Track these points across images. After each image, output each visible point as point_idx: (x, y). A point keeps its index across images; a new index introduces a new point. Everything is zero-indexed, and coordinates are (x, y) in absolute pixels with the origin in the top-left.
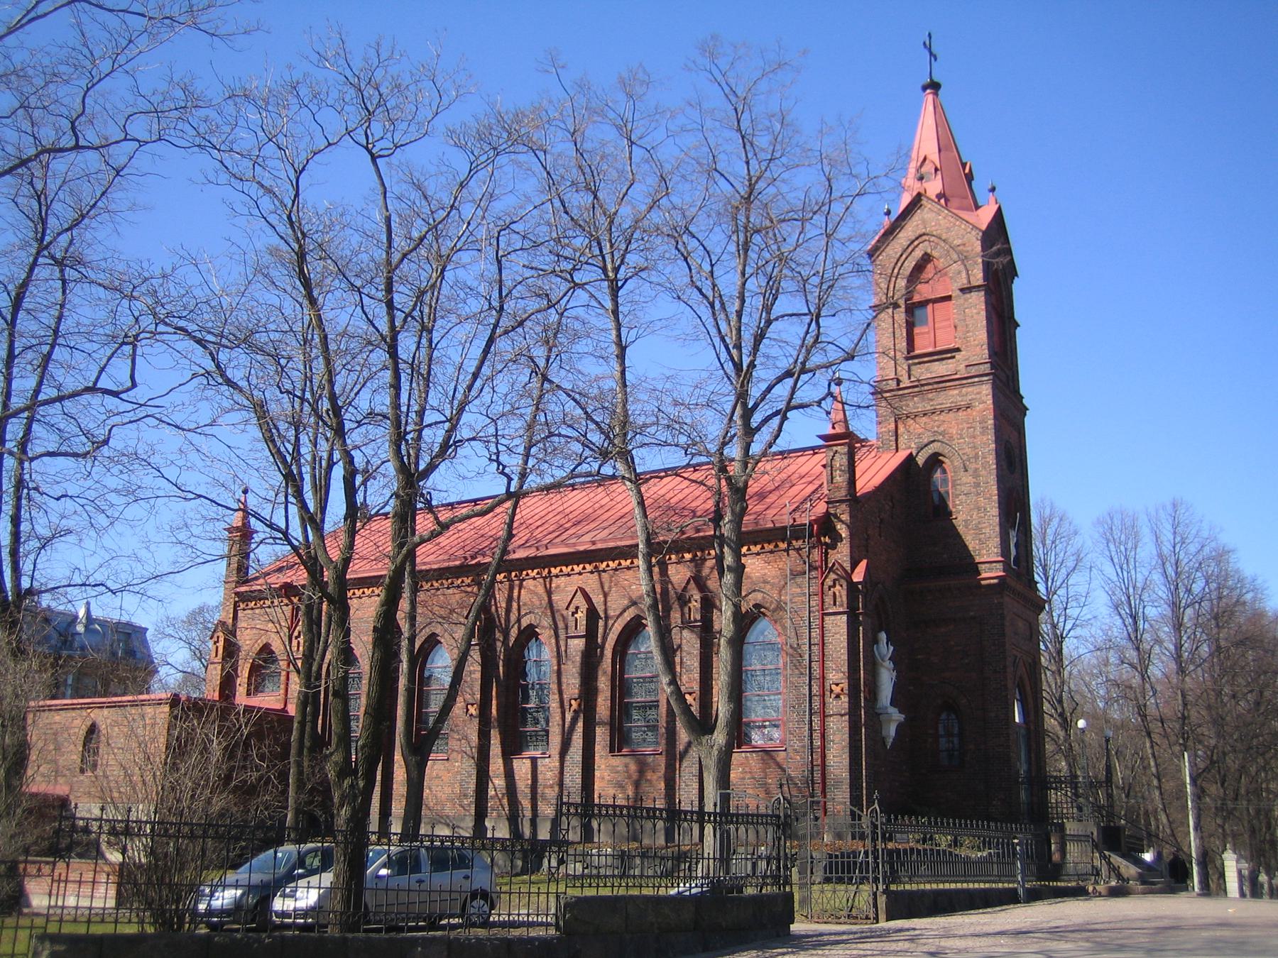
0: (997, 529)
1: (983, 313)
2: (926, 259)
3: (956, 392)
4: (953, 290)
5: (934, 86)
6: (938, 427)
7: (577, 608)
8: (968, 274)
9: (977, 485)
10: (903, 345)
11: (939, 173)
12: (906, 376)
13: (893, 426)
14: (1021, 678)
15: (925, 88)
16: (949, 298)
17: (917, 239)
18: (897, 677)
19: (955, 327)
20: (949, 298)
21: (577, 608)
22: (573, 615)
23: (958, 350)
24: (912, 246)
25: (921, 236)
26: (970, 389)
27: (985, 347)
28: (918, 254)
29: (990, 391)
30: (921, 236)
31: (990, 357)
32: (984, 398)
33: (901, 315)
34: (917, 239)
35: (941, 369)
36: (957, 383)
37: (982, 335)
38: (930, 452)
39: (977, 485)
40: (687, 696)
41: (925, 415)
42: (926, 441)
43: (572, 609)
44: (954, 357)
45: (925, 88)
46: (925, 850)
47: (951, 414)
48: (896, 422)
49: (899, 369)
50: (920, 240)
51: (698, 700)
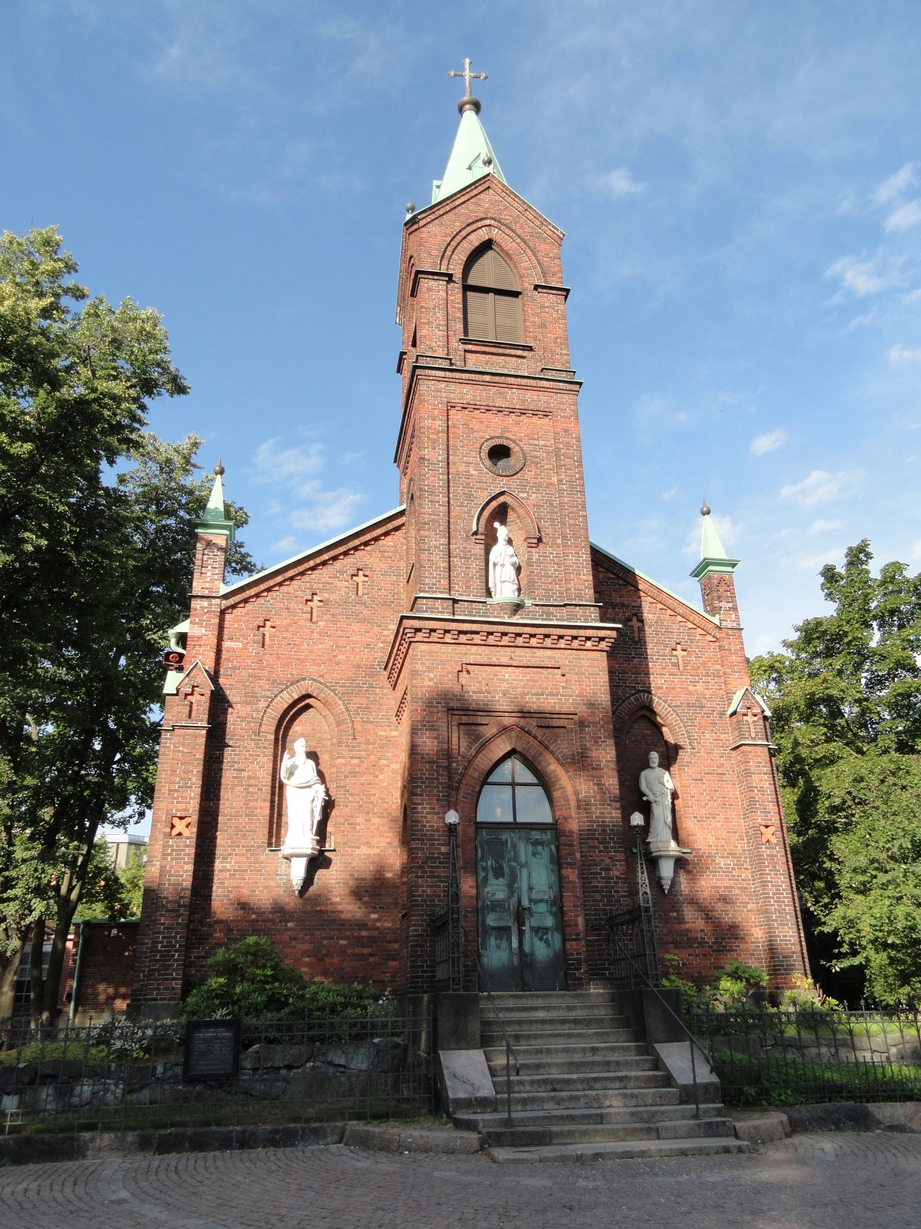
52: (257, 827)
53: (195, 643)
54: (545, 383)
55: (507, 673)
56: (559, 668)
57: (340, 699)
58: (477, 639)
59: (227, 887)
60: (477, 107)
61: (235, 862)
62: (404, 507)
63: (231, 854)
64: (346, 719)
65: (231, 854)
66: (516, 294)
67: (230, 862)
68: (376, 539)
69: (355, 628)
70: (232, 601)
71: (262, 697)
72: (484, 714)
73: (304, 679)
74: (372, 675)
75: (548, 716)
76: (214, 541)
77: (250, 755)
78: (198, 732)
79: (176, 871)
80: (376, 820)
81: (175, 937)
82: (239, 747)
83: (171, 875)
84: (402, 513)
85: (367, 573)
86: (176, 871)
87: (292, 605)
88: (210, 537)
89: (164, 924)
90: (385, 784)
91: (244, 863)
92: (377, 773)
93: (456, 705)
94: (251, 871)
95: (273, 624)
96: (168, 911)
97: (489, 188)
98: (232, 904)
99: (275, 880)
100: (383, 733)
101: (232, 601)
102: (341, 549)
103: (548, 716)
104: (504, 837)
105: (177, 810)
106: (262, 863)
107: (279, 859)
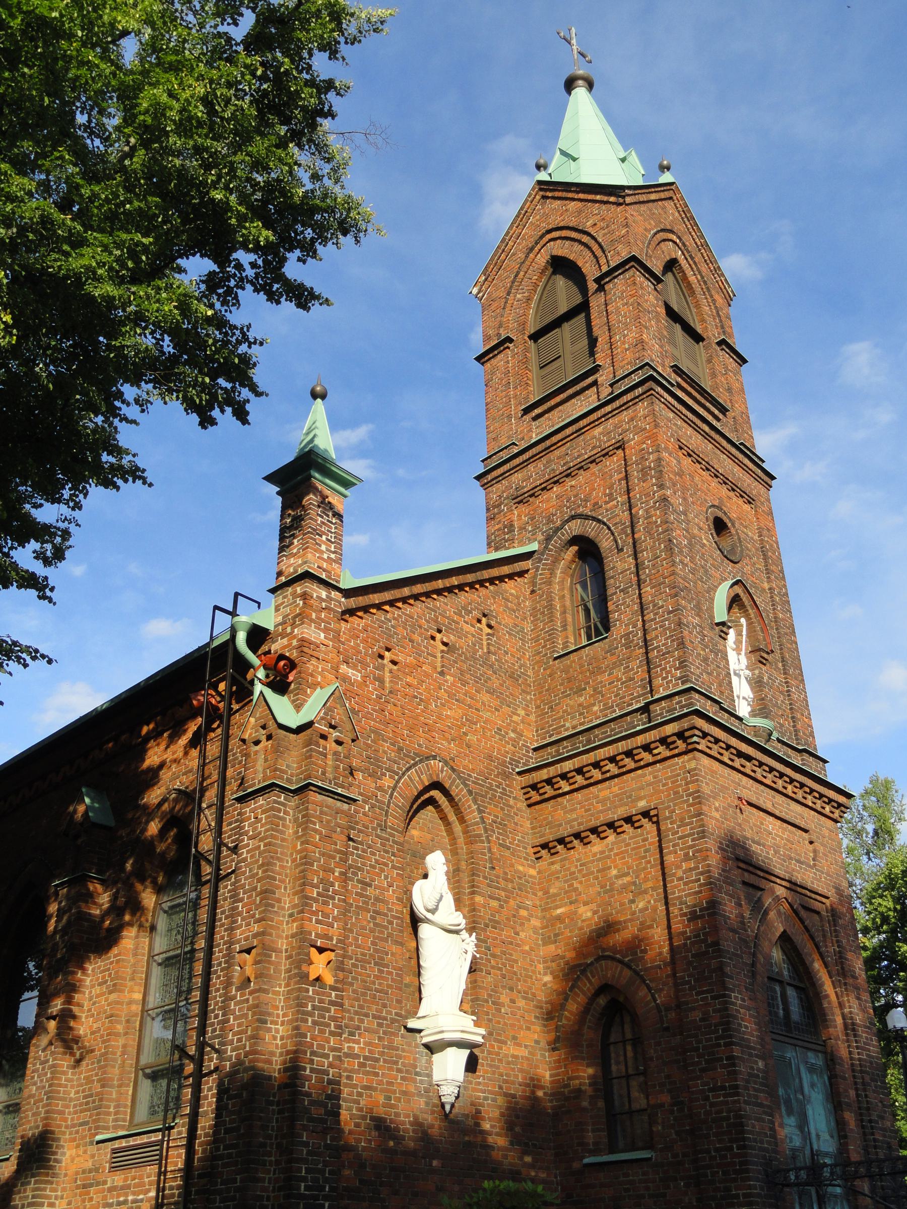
52: (389, 986)
53: (311, 652)
54: (746, 461)
55: (771, 824)
56: (806, 831)
57: (475, 801)
58: (749, 767)
59: (356, 1086)
60: (590, 85)
61: (365, 1043)
62: (534, 546)
63: (359, 1028)
64: (480, 836)
65: (359, 1028)
66: (698, 338)
67: (358, 1042)
68: (501, 579)
69: (485, 699)
70: (362, 601)
71: (388, 770)
72: (762, 874)
73: (434, 758)
74: (506, 776)
75: (808, 893)
76: (330, 499)
77: (377, 861)
78: (339, 804)
79: (319, 1046)
80: (521, 1003)
81: (322, 1172)
82: (361, 843)
83: (313, 1053)
84: (528, 555)
85: (493, 623)
86: (319, 1046)
87: (416, 637)
88: (327, 492)
89: (306, 1144)
90: (527, 948)
91: (377, 1046)
92: (518, 928)
93: (740, 853)
94: (385, 1061)
95: (395, 658)
96: (311, 1119)
97: (671, 198)
98: (364, 1118)
99: (415, 1081)
100: (521, 868)
101: (362, 601)
102: (470, 578)
103: (808, 893)
104: (788, 1055)
105: (317, 935)
106: (397, 1049)
107: (417, 1046)
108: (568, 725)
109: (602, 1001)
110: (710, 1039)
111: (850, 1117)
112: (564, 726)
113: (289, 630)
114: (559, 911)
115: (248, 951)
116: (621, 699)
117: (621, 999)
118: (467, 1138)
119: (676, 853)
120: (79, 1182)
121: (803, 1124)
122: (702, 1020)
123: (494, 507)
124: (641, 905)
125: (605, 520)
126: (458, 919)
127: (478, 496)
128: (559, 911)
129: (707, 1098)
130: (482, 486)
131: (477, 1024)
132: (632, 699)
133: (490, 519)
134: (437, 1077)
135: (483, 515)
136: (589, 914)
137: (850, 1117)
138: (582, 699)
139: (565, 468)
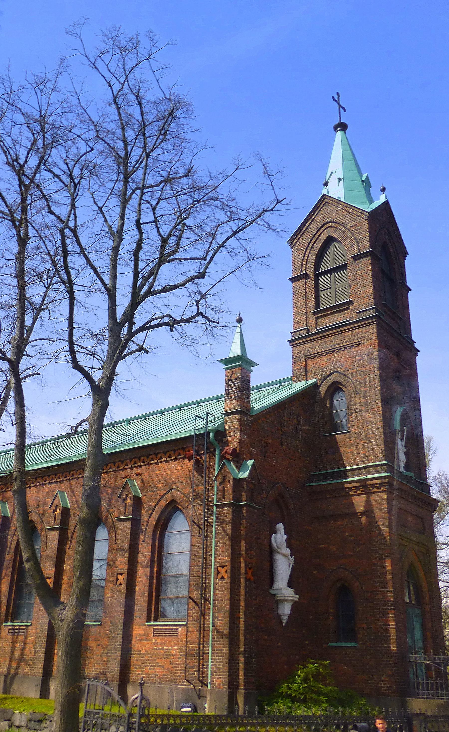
0: (382, 438)
1: (370, 273)
2: (330, 240)
3: (350, 333)
4: (347, 259)
5: (342, 127)
6: (337, 361)
7: (56, 507)
8: (358, 245)
9: (366, 404)
10: (312, 303)
11: (342, 182)
12: (314, 326)
13: (304, 364)
14: (411, 566)
15: (335, 128)
16: (344, 267)
17: (322, 226)
18: (295, 562)
19: (350, 286)
20: (344, 267)
21: (56, 507)
22: (53, 512)
23: (351, 302)
24: (319, 233)
25: (325, 224)
26: (360, 330)
27: (372, 297)
28: (323, 237)
29: (375, 329)
30: (325, 224)
31: (375, 304)
32: (371, 336)
33: (311, 282)
34: (322, 226)
35: (340, 318)
36: (350, 327)
37: (370, 289)
38: (331, 381)
39: (366, 404)
40: (48, 580)
41: (327, 353)
42: (328, 373)
43: (53, 508)
44: (348, 308)
45: (335, 128)
46: (428, 683)
47: (346, 351)
48: (306, 361)
49: (309, 321)
50: (325, 227)
51: (229, 573)
108: (328, 467)
109: (338, 584)
110: (384, 606)
111: (429, 634)
112: (327, 467)
113: (232, 434)
114: (322, 546)
115: (223, 567)
116: (353, 460)
117: (347, 585)
118: (289, 635)
119: (375, 531)
120: (138, 639)
121: (413, 637)
122: (382, 599)
123: (296, 357)
124: (358, 549)
125: (350, 377)
126: (288, 552)
127: (288, 348)
128: (322, 546)
129: (382, 628)
130: (291, 346)
131: (296, 593)
132: (359, 462)
133: (294, 363)
134: (280, 612)
135: (291, 361)
136: (335, 549)
137: (429, 634)
138: (335, 457)
139: (332, 347)
